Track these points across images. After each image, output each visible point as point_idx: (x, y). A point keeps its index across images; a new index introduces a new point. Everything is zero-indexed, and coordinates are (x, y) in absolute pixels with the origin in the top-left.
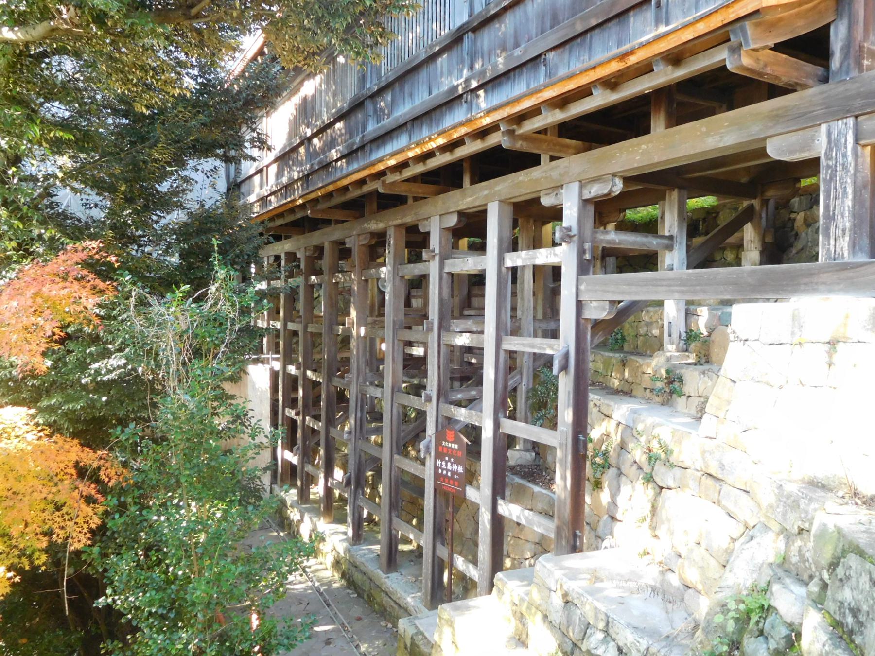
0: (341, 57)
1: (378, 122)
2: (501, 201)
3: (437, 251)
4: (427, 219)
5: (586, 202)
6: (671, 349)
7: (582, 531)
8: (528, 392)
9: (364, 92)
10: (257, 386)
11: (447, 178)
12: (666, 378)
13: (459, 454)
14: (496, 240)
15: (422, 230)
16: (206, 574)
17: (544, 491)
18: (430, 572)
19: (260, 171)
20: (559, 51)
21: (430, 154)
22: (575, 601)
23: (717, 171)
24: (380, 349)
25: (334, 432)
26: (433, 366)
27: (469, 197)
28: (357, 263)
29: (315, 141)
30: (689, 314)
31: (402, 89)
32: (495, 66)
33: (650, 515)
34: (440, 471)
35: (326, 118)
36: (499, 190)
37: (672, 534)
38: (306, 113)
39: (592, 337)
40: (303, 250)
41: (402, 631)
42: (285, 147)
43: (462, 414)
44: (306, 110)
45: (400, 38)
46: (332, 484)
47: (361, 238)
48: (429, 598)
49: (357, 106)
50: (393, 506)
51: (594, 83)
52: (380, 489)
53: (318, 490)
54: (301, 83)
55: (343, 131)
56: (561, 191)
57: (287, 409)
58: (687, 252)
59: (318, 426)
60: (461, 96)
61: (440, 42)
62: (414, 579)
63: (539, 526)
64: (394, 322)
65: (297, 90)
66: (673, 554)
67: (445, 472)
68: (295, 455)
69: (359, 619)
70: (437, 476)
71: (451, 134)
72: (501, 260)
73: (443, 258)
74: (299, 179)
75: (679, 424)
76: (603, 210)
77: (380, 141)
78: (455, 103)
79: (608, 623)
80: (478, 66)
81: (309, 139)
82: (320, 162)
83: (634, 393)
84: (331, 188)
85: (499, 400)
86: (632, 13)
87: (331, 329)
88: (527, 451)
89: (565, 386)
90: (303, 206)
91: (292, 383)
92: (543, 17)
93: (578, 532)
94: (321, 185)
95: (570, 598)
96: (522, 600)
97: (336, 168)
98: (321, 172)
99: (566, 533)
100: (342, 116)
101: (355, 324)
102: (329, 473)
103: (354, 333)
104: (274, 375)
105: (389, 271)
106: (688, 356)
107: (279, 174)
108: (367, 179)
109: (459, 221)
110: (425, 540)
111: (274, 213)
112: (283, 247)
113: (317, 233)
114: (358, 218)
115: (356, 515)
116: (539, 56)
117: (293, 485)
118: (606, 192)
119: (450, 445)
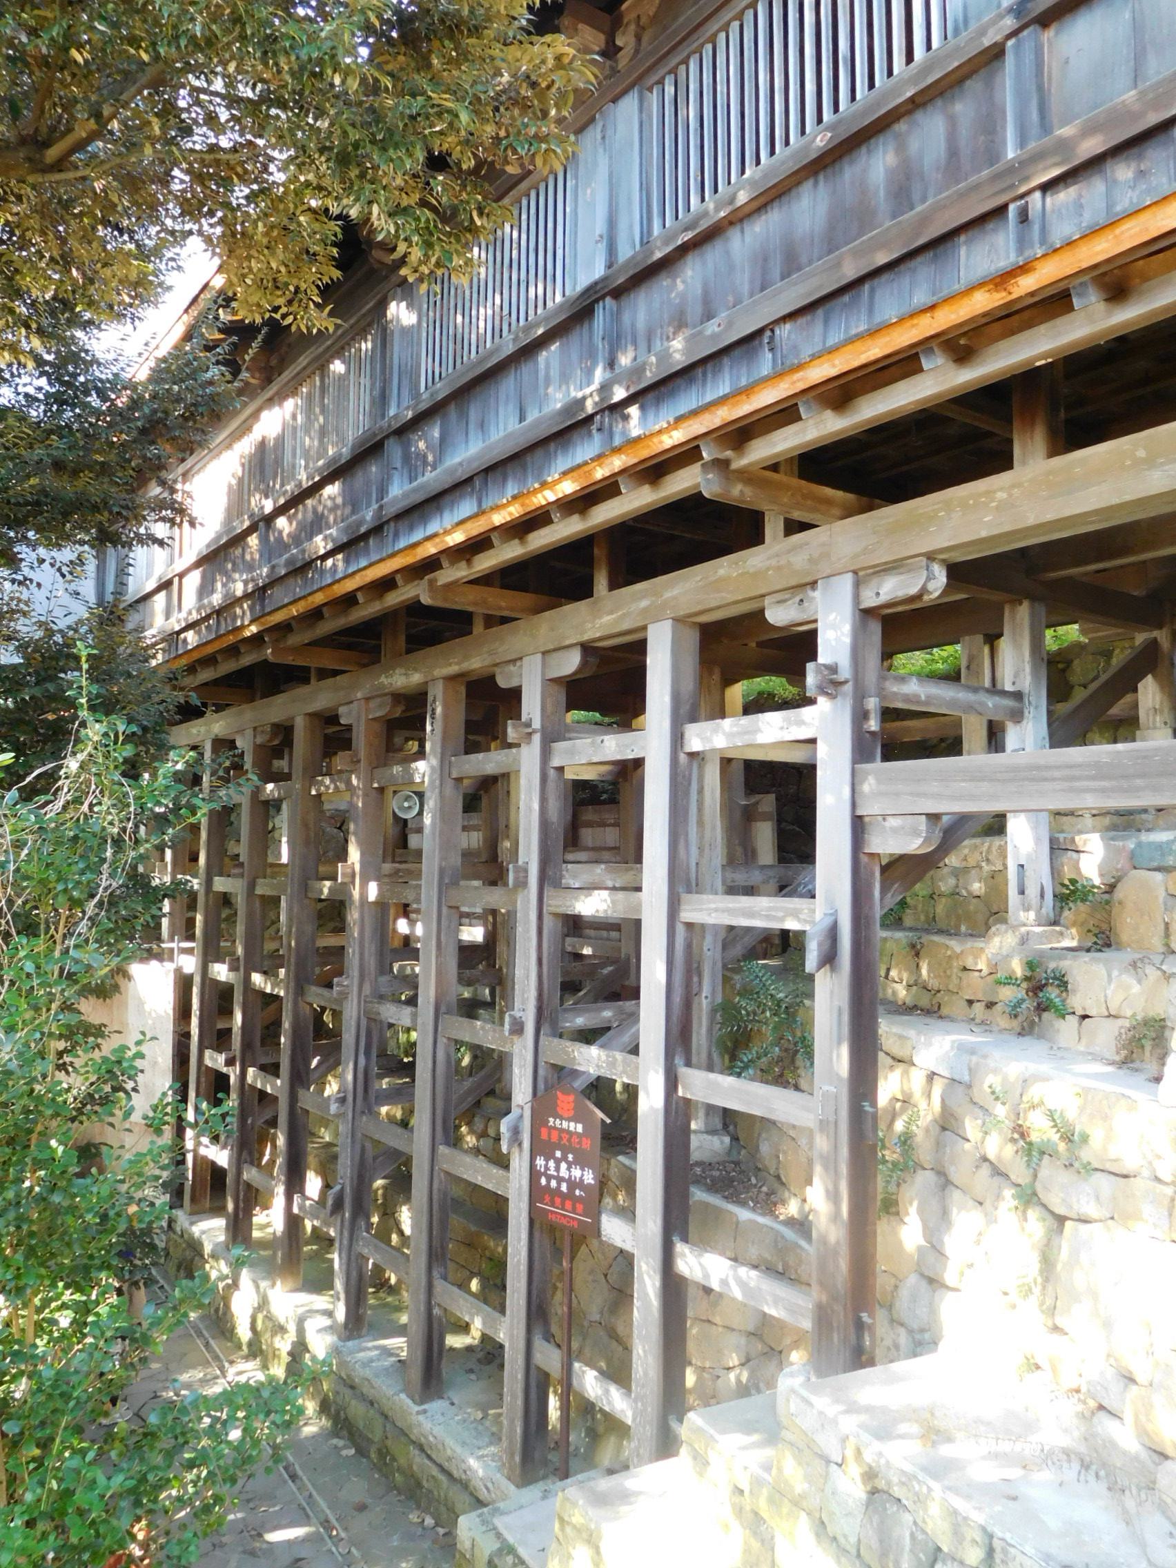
0: (337, 362)
1: (411, 479)
2: (676, 620)
3: (537, 724)
4: (514, 661)
5: (867, 613)
6: (1026, 917)
7: (872, 1316)
8: (714, 1011)
9: (384, 423)
10: (147, 1008)
11: (558, 577)
12: (1027, 979)
13: (587, 1144)
14: (667, 699)
15: (503, 683)
16: (29, 1497)
17: (761, 1220)
18: (520, 1402)
19: (166, 585)
20: (802, 321)
21: (536, 520)
22: (897, 1491)
23: (1100, 566)
24: (395, 931)
25: (307, 1098)
26: (528, 958)
27: (606, 614)
28: (362, 755)
29: (282, 522)
30: (1058, 848)
31: (463, 415)
32: (664, 356)
33: (1039, 1280)
34: (543, 1181)
35: (304, 478)
36: (674, 598)
37: (1107, 1325)
38: (262, 471)
39: (884, 891)
40: (249, 732)
41: (467, 1545)
42: (218, 537)
43: (592, 1060)
44: (264, 465)
45: (459, 318)
46: (301, 1207)
47: (372, 704)
48: (517, 1459)
49: (369, 451)
50: (436, 1255)
51: (925, 344)
52: (406, 1217)
53: (270, 1220)
54: (255, 415)
55: (339, 500)
56: (811, 593)
57: (208, 1053)
58: (1050, 724)
59: (275, 1086)
60: (590, 419)
61: (546, 319)
62: (480, 1415)
63: (777, 1301)
64: (442, 871)
65: (245, 429)
66: (1110, 1373)
67: (554, 1184)
68: (224, 1147)
69: (362, 1508)
70: (536, 1192)
71: (589, 473)
72: (678, 739)
73: (551, 737)
74: (247, 596)
75: (1088, 1076)
76: (898, 628)
77: (416, 515)
78: (575, 436)
79: (990, 1552)
80: (625, 360)
81: (269, 520)
82: (289, 562)
83: (945, 1011)
84: (319, 598)
85: (675, 1030)
86: (963, 238)
87: (305, 887)
88: (712, 1132)
89: (829, 999)
90: (257, 640)
91: (220, 998)
92: (765, 260)
93: (865, 1316)
94: (290, 604)
95: (881, 1484)
96: (757, 1482)
97: (322, 572)
98: (291, 581)
99: (840, 1314)
100: (337, 472)
101: (359, 878)
102: (295, 1183)
103: (356, 894)
104: (184, 984)
105: (432, 768)
106: (1061, 934)
107: (205, 589)
108: (398, 577)
109: (584, 664)
110: (509, 1331)
111: (196, 656)
112: (214, 726)
113: (280, 699)
114: (365, 666)
115: (354, 1274)
116: (759, 333)
117: (218, 1210)
118: (913, 591)
119: (565, 1124)
